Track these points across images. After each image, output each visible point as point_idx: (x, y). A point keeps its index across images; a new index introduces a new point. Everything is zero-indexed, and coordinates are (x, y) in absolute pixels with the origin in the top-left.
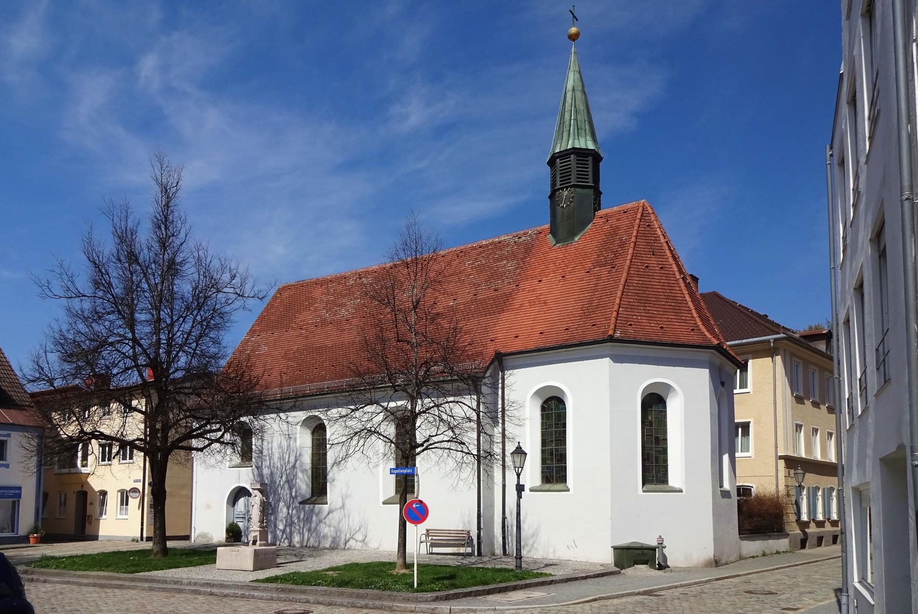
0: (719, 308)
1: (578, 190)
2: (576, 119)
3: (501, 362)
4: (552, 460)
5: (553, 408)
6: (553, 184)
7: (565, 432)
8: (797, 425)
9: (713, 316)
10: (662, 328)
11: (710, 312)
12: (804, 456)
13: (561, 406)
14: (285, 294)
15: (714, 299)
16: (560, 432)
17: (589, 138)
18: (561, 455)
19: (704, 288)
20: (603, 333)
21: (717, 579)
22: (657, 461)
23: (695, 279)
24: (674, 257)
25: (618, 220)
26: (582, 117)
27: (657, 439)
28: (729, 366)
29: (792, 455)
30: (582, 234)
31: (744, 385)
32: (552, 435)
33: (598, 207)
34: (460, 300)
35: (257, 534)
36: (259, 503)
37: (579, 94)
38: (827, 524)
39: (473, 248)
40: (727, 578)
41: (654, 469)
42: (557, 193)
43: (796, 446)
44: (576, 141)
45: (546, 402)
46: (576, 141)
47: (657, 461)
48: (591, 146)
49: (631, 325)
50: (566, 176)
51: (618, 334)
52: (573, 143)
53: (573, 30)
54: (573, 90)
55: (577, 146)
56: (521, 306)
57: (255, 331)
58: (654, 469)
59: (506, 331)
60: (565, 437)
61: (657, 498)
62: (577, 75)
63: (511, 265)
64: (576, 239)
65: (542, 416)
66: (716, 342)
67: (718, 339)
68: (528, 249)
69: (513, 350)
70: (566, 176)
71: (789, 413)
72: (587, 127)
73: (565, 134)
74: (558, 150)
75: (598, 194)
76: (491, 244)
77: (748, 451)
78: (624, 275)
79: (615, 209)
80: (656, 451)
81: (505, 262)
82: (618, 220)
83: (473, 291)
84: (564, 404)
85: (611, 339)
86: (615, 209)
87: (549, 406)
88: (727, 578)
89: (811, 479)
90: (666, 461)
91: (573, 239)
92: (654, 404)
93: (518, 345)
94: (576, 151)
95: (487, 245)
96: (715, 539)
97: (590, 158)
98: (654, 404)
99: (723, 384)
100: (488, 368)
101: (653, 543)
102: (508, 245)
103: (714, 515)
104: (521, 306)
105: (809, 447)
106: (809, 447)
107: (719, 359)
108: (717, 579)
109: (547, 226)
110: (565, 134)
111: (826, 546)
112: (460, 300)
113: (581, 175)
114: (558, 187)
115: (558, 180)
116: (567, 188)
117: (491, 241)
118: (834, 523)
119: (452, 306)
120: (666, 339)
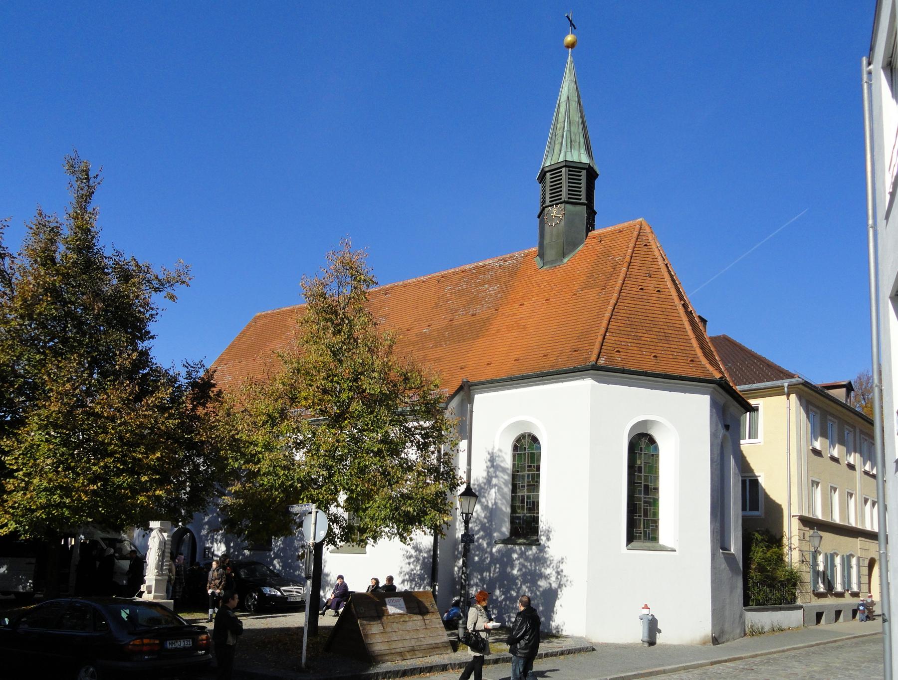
2: (569, 131)
3: (466, 391)
4: (523, 508)
5: (527, 449)
6: (544, 202)
7: (538, 476)
8: (813, 482)
9: (722, 360)
10: (655, 356)
11: (715, 347)
12: (820, 518)
13: (535, 445)
14: (260, 323)
15: (726, 345)
16: (533, 475)
17: (583, 151)
18: (534, 502)
19: (711, 332)
20: (586, 359)
21: (712, 664)
22: (646, 515)
23: (704, 321)
24: (673, 281)
25: (612, 240)
26: (577, 129)
27: (647, 488)
28: (734, 407)
29: (807, 515)
30: (571, 255)
31: (753, 435)
32: (523, 479)
35: (153, 583)
36: (723, 560)
37: (574, 105)
38: (847, 594)
39: (455, 273)
40: (726, 661)
41: (641, 523)
42: (547, 209)
44: (569, 154)
45: (518, 440)
46: (569, 154)
47: (646, 515)
48: (585, 159)
49: (618, 351)
51: (601, 362)
52: (565, 156)
53: (569, 38)
54: (568, 100)
57: (223, 359)
58: (641, 523)
59: (474, 360)
60: (538, 482)
61: (643, 556)
62: (573, 85)
63: (493, 289)
64: (565, 260)
66: (718, 376)
67: (721, 372)
69: (483, 379)
71: (804, 468)
72: (582, 139)
75: (591, 213)
78: (615, 295)
80: (645, 502)
81: (487, 286)
82: (612, 240)
83: (449, 317)
84: (539, 443)
88: (726, 661)
89: (830, 541)
90: (656, 514)
91: (562, 261)
94: (568, 165)
95: (470, 270)
97: (584, 172)
98: (642, 448)
99: (727, 427)
102: (493, 268)
103: (712, 582)
105: (828, 506)
106: (828, 506)
107: (724, 398)
108: (712, 664)
109: (535, 249)
111: (845, 621)
112: (434, 327)
113: (573, 190)
114: (548, 203)
115: (548, 196)
116: (557, 204)
117: (475, 264)
118: (855, 595)
120: (658, 371)
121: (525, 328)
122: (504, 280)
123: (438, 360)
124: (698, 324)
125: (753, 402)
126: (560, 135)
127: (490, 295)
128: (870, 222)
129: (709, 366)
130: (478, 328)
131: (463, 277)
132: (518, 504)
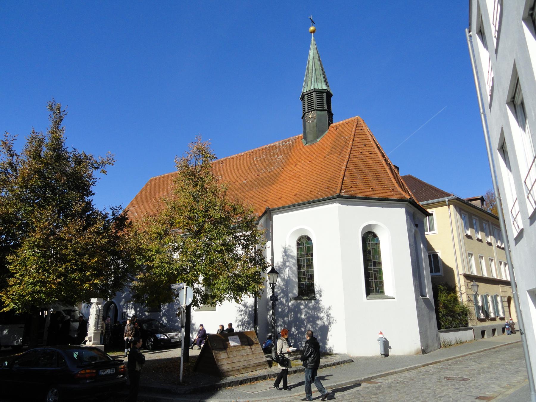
0: (412, 182)
1: (318, 112)
2: (315, 74)
5: (305, 244)
6: (304, 110)
7: (312, 259)
8: (469, 254)
12: (476, 274)
14: (153, 183)
15: (410, 179)
16: (309, 259)
17: (323, 83)
18: (311, 275)
19: (402, 173)
21: (424, 366)
22: (375, 278)
23: (397, 168)
25: (343, 128)
27: (374, 262)
28: (419, 214)
30: (321, 137)
32: (304, 261)
33: (330, 121)
34: (249, 180)
37: (317, 61)
38: (498, 319)
40: (431, 364)
41: (373, 283)
43: (470, 267)
47: (375, 278)
48: (325, 87)
49: (351, 187)
50: (310, 105)
51: (343, 193)
53: (312, 28)
54: (313, 58)
55: (316, 88)
56: (284, 180)
58: (373, 283)
61: (375, 303)
62: (316, 51)
63: (280, 158)
64: (318, 140)
65: (298, 249)
66: (408, 197)
67: (410, 195)
68: (290, 148)
69: (278, 206)
70: (310, 105)
73: (309, 82)
74: (305, 91)
75: (330, 115)
76: (269, 147)
77: (439, 271)
79: (341, 122)
80: (374, 271)
82: (343, 128)
85: (340, 197)
86: (341, 122)
87: (302, 242)
88: (431, 364)
92: (369, 240)
93: (281, 204)
94: (316, 91)
95: (267, 148)
96: (421, 333)
97: (325, 94)
98: (369, 240)
99: (416, 226)
100: (261, 218)
101: (219, 328)
102: (279, 147)
104: (284, 180)
105: (479, 267)
106: (479, 267)
107: (413, 209)
108: (424, 366)
109: (302, 135)
110: (309, 82)
112: (249, 180)
113: (320, 104)
115: (306, 107)
117: (269, 145)
118: (502, 319)
119: (244, 183)
120: (375, 196)
121: (299, 177)
122: (286, 152)
123: (252, 197)
124: (394, 170)
125: (429, 211)
126: (310, 76)
127: (278, 161)
128: (481, 111)
129: (402, 192)
130: (273, 179)
131: (263, 152)
132: (302, 276)
